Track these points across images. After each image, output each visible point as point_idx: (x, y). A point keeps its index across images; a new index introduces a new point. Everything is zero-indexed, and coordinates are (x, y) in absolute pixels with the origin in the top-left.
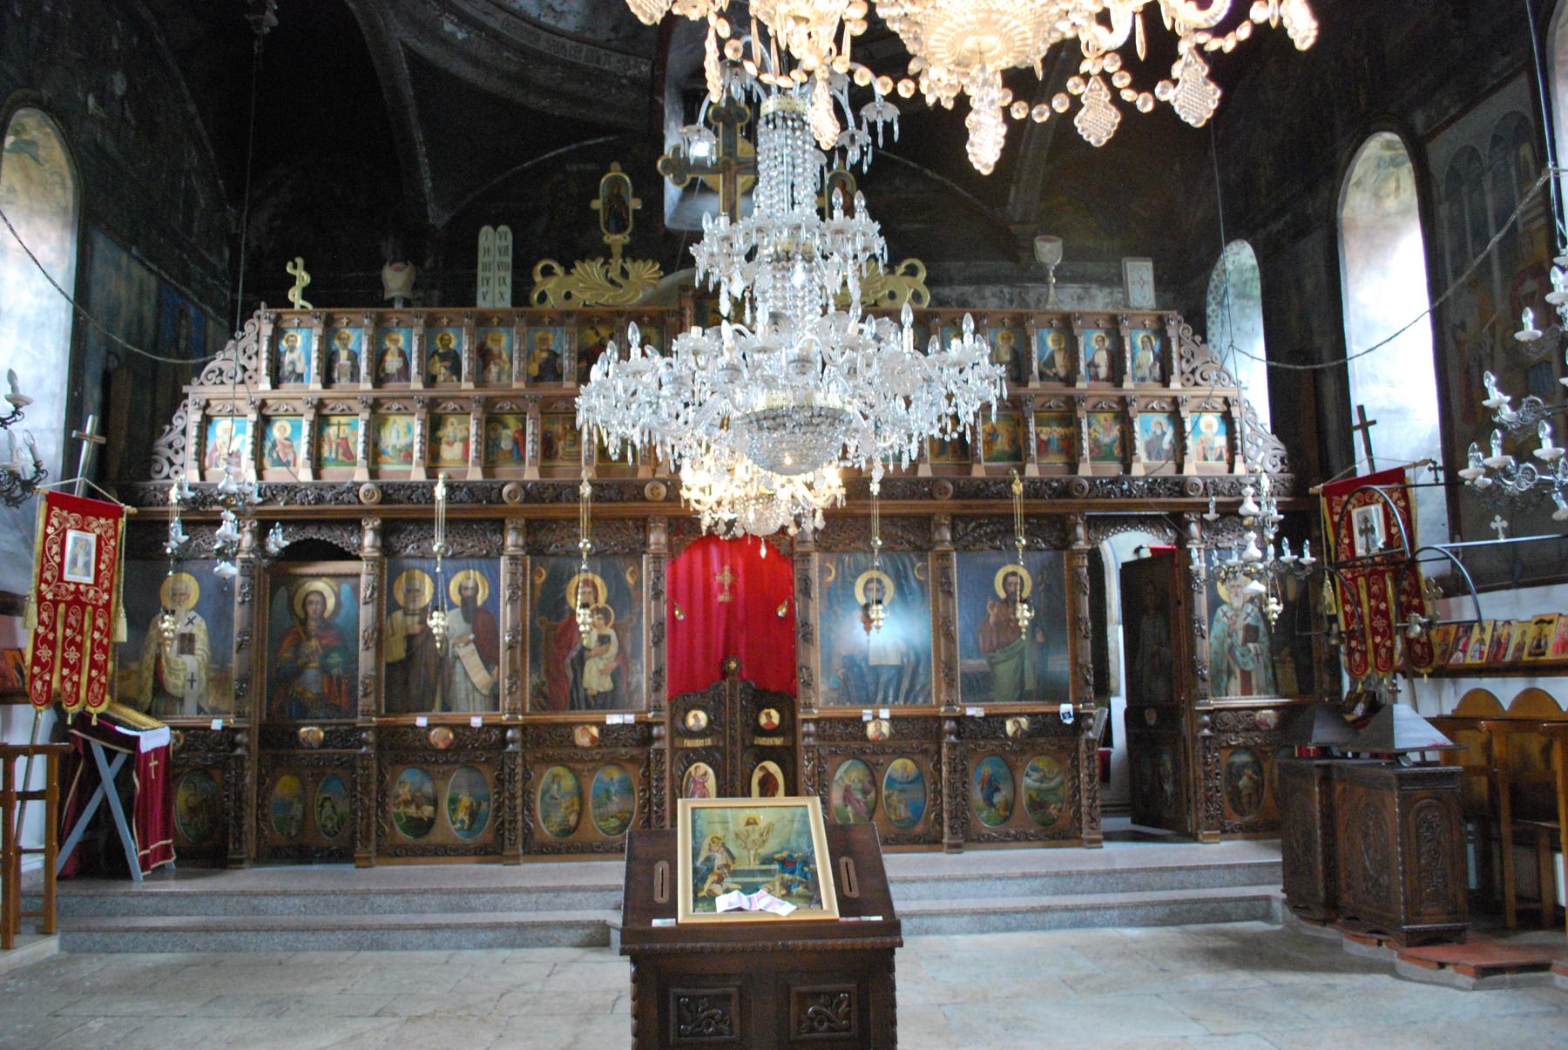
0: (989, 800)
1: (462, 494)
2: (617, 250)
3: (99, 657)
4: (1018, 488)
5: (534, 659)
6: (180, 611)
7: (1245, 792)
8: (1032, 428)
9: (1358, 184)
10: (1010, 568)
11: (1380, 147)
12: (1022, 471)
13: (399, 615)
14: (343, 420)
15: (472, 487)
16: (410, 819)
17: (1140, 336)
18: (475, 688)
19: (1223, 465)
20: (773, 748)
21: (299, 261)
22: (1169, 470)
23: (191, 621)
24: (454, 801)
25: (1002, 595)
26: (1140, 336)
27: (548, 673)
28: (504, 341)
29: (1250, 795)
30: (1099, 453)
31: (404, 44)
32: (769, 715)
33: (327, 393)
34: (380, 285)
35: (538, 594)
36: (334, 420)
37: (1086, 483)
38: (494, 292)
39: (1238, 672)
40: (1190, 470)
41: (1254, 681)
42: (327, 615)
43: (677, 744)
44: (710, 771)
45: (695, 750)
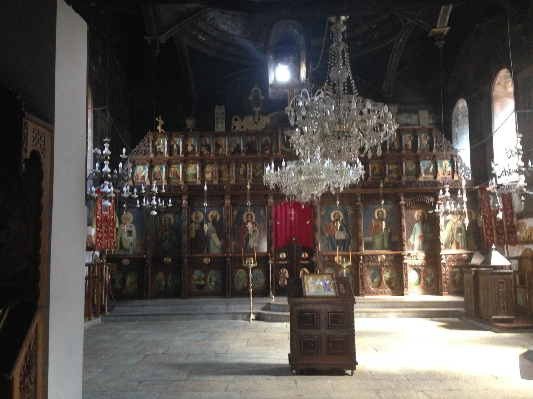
0: (373, 281)
1: (212, 188)
2: (257, 112)
3: (112, 235)
4: (382, 185)
5: (234, 237)
6: (128, 223)
7: (457, 281)
8: (387, 166)
9: (499, 84)
10: (380, 209)
11: (504, 73)
12: (383, 180)
13: (193, 224)
14: (175, 166)
15: (215, 186)
16: (197, 285)
17: (423, 136)
18: (217, 247)
19: (450, 176)
20: (306, 264)
21: (160, 117)
22: (431, 177)
23: (131, 227)
24: (211, 279)
25: (377, 217)
26: (423, 136)
27: (238, 242)
28: (223, 142)
29: (459, 282)
30: (408, 173)
31: (187, 45)
32: (305, 254)
33: (170, 158)
34: (185, 125)
35: (235, 217)
36: (173, 166)
37: (404, 183)
38: (220, 127)
39: (455, 243)
40: (439, 178)
41: (460, 245)
42: (171, 224)
43: (277, 263)
44: (287, 271)
45: (282, 265)
